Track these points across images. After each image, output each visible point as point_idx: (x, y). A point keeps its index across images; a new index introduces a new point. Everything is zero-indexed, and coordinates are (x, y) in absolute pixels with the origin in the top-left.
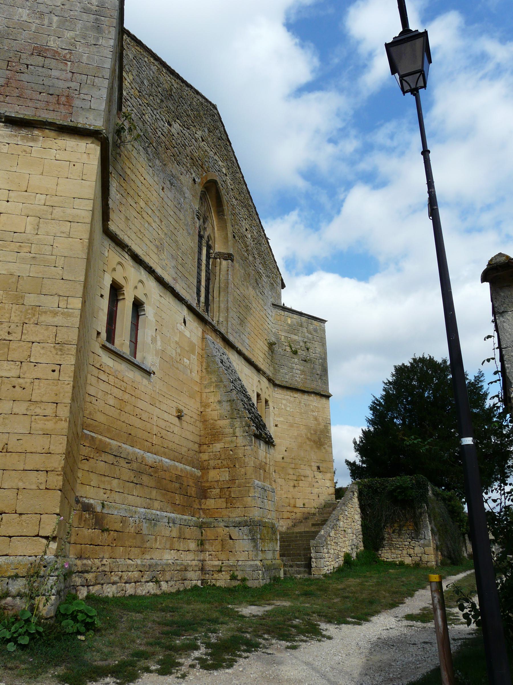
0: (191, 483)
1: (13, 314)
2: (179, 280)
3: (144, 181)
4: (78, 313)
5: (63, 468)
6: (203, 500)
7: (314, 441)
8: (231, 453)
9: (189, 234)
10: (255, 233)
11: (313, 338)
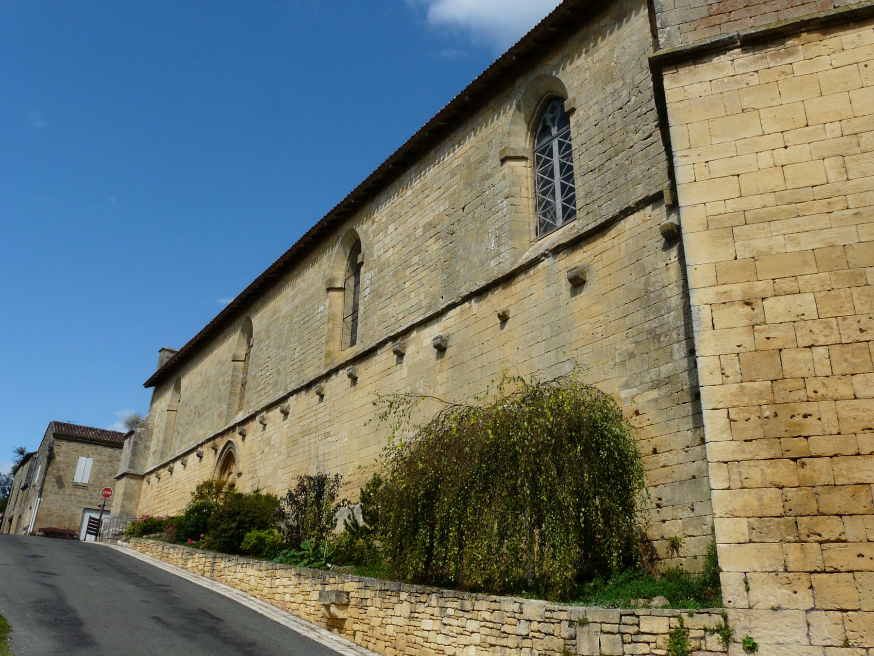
1: (857, 303)
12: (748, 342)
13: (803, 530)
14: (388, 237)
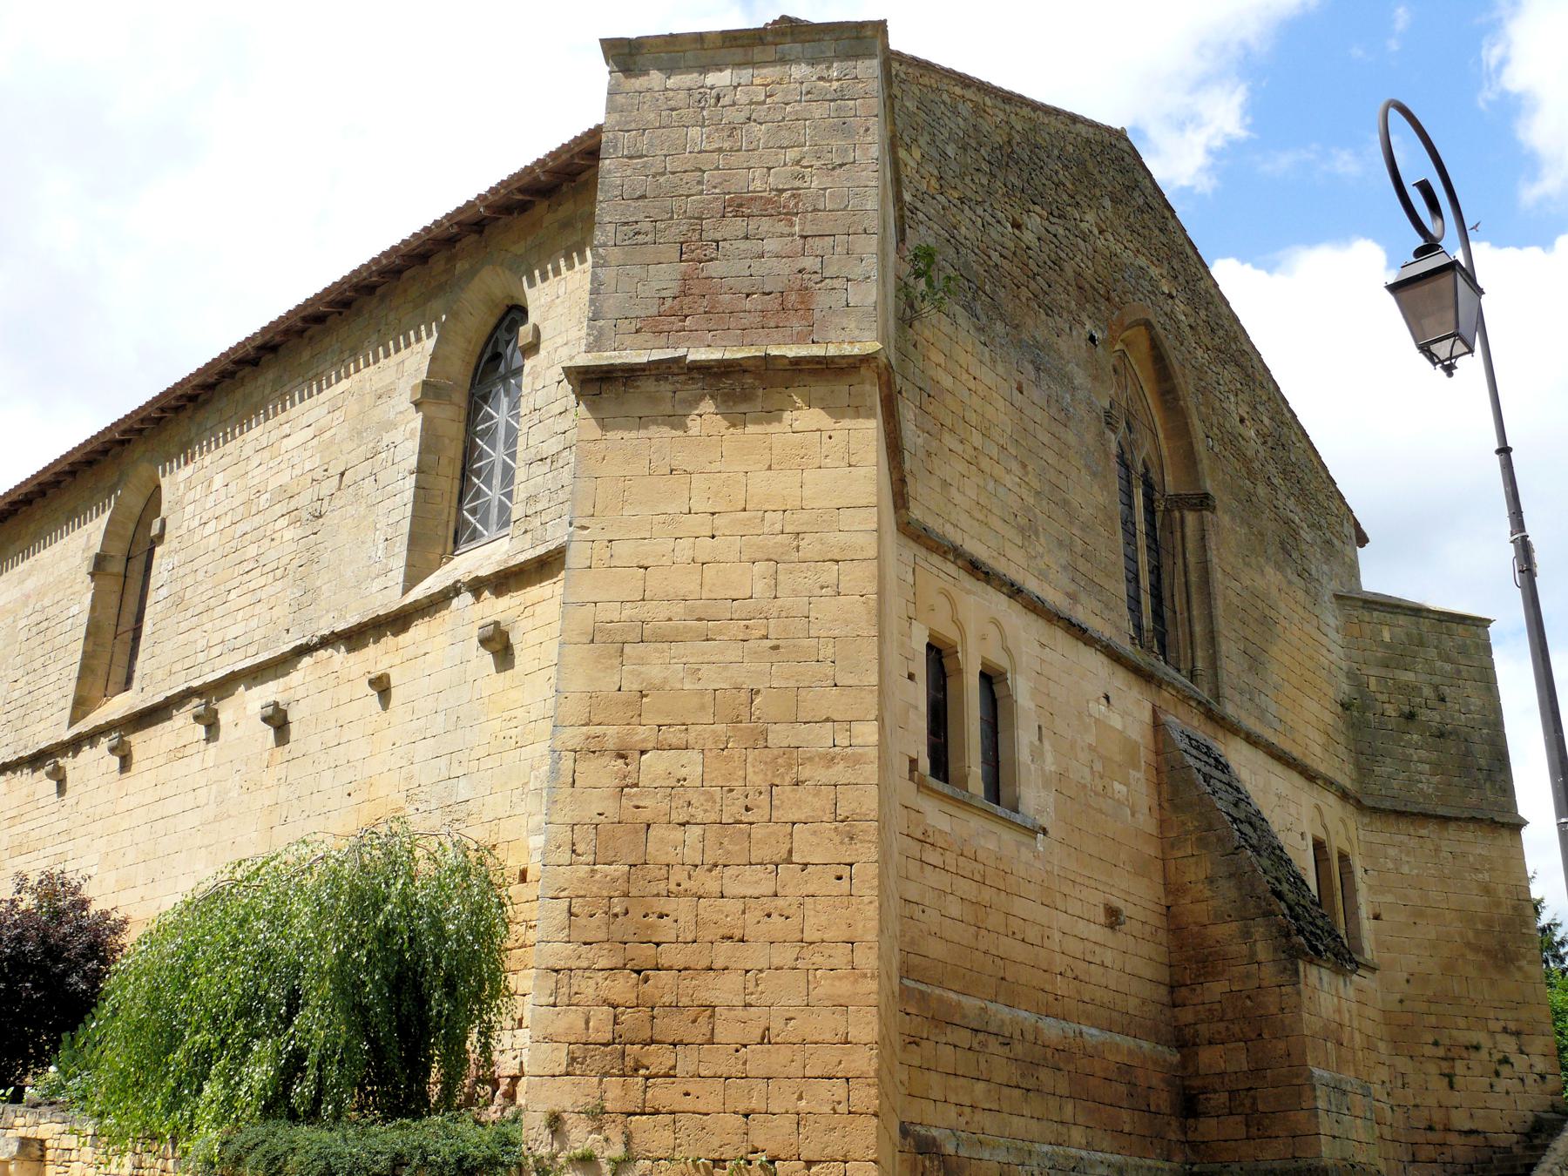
0: (1155, 1082)
1: (750, 770)
2: (1083, 597)
3: (972, 384)
4: (873, 753)
5: (878, 1071)
6: (1191, 1121)
7: (1487, 952)
8: (1248, 1003)
9: (1094, 474)
10: (1266, 421)
11: (1459, 672)
12: (610, 807)
13: (630, 1062)
14: (212, 498)
